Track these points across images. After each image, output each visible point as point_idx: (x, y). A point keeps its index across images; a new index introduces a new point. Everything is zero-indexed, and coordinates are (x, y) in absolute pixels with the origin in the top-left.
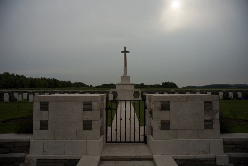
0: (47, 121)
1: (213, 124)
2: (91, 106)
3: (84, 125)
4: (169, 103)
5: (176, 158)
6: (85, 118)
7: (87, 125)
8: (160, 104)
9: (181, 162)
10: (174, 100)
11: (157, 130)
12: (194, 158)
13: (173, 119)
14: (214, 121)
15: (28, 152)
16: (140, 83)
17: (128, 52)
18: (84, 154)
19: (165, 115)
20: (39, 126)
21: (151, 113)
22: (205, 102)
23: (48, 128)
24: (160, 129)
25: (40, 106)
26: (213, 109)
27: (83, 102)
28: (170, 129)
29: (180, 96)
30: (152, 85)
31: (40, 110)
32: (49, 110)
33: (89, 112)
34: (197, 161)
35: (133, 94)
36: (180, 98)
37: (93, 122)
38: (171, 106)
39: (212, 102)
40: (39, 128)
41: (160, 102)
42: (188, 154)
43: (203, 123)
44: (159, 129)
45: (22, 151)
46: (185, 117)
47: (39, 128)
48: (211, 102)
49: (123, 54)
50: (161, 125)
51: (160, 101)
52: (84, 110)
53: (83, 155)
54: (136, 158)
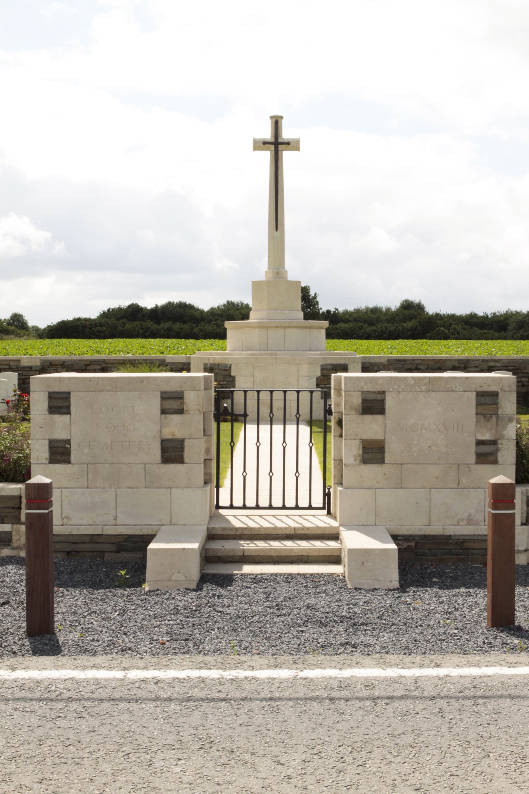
0: (68, 442)
1: (497, 450)
2: (182, 403)
3: (164, 450)
4: (383, 396)
5: (396, 533)
6: (167, 434)
7: (172, 452)
8: (361, 397)
9: (410, 544)
10: (396, 387)
11: (353, 464)
12: (442, 534)
13: (393, 437)
14: (502, 444)
15: (234, 387)
16: (391, 301)
17: (293, 145)
18: (164, 523)
19: (372, 427)
20: (47, 455)
21: (340, 423)
22: (480, 395)
23: (69, 458)
24: (360, 462)
25: (49, 402)
26: (500, 412)
27: (162, 393)
28: (386, 462)
29: (412, 377)
30: (485, 317)
31: (47, 413)
32: (72, 413)
33: (175, 418)
34: (451, 541)
35: (318, 379)
36: (413, 382)
37: (186, 443)
38: (389, 403)
39: (498, 393)
40: (47, 459)
41: (360, 393)
42: (429, 525)
43: (473, 449)
44: (357, 462)
45: (3, 519)
46: (424, 431)
47: (47, 459)
48: (495, 394)
49: (266, 156)
50: (361, 452)
51: (360, 391)
52: (164, 412)
53: (162, 525)
54: (298, 532)
